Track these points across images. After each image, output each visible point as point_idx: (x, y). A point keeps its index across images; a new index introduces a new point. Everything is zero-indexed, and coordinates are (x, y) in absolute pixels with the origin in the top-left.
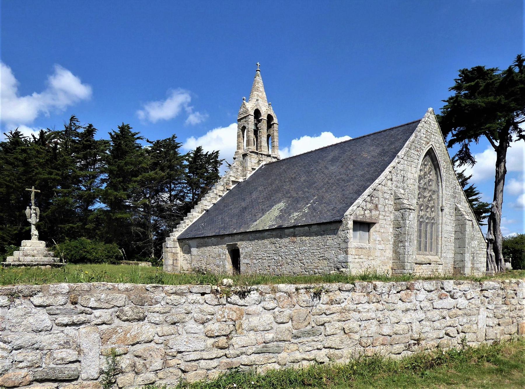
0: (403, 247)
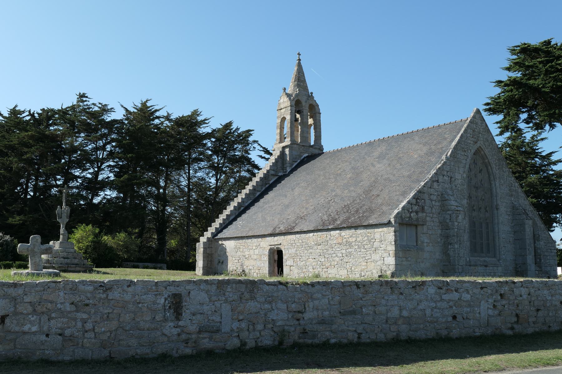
0: (453, 250)
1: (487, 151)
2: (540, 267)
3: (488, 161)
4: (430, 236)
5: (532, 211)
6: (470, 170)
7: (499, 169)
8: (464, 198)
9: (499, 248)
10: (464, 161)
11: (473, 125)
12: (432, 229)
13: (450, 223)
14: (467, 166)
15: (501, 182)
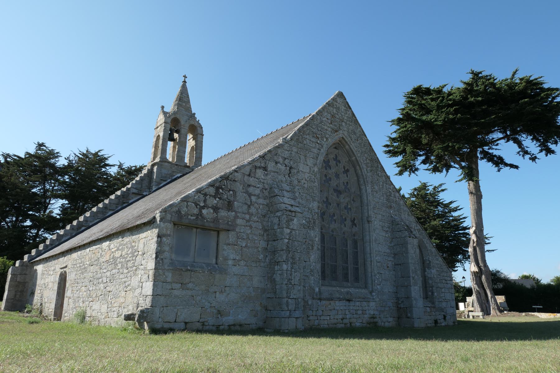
0: (279, 272)
1: (353, 146)
2: (433, 303)
3: (356, 158)
4: (241, 250)
5: (419, 230)
6: (326, 164)
7: (371, 171)
8: (314, 200)
9: (372, 275)
10: (315, 151)
11: (332, 108)
12: (248, 238)
13: (279, 230)
14: (321, 158)
15: (374, 188)
